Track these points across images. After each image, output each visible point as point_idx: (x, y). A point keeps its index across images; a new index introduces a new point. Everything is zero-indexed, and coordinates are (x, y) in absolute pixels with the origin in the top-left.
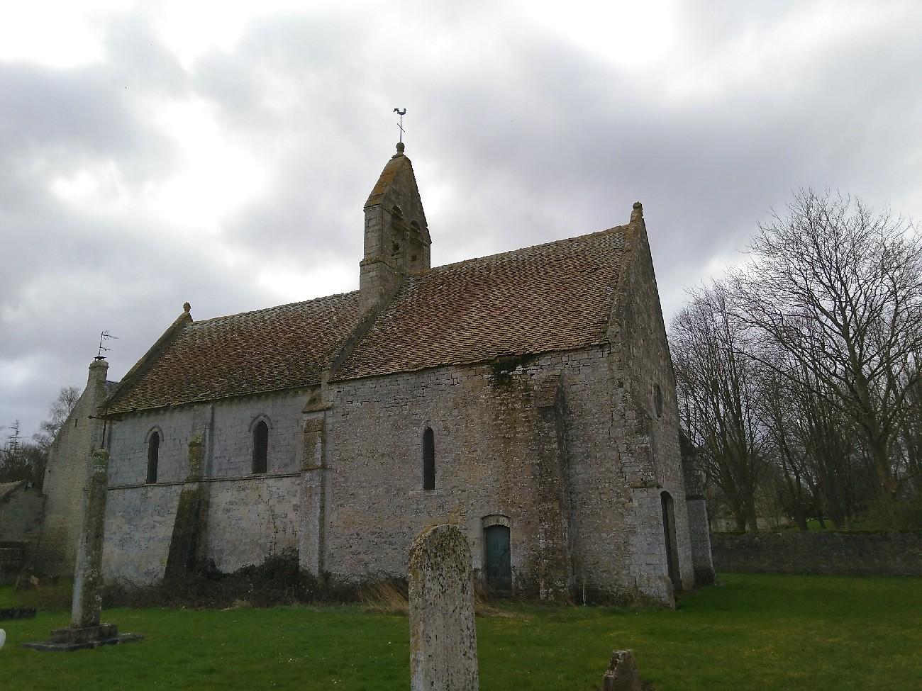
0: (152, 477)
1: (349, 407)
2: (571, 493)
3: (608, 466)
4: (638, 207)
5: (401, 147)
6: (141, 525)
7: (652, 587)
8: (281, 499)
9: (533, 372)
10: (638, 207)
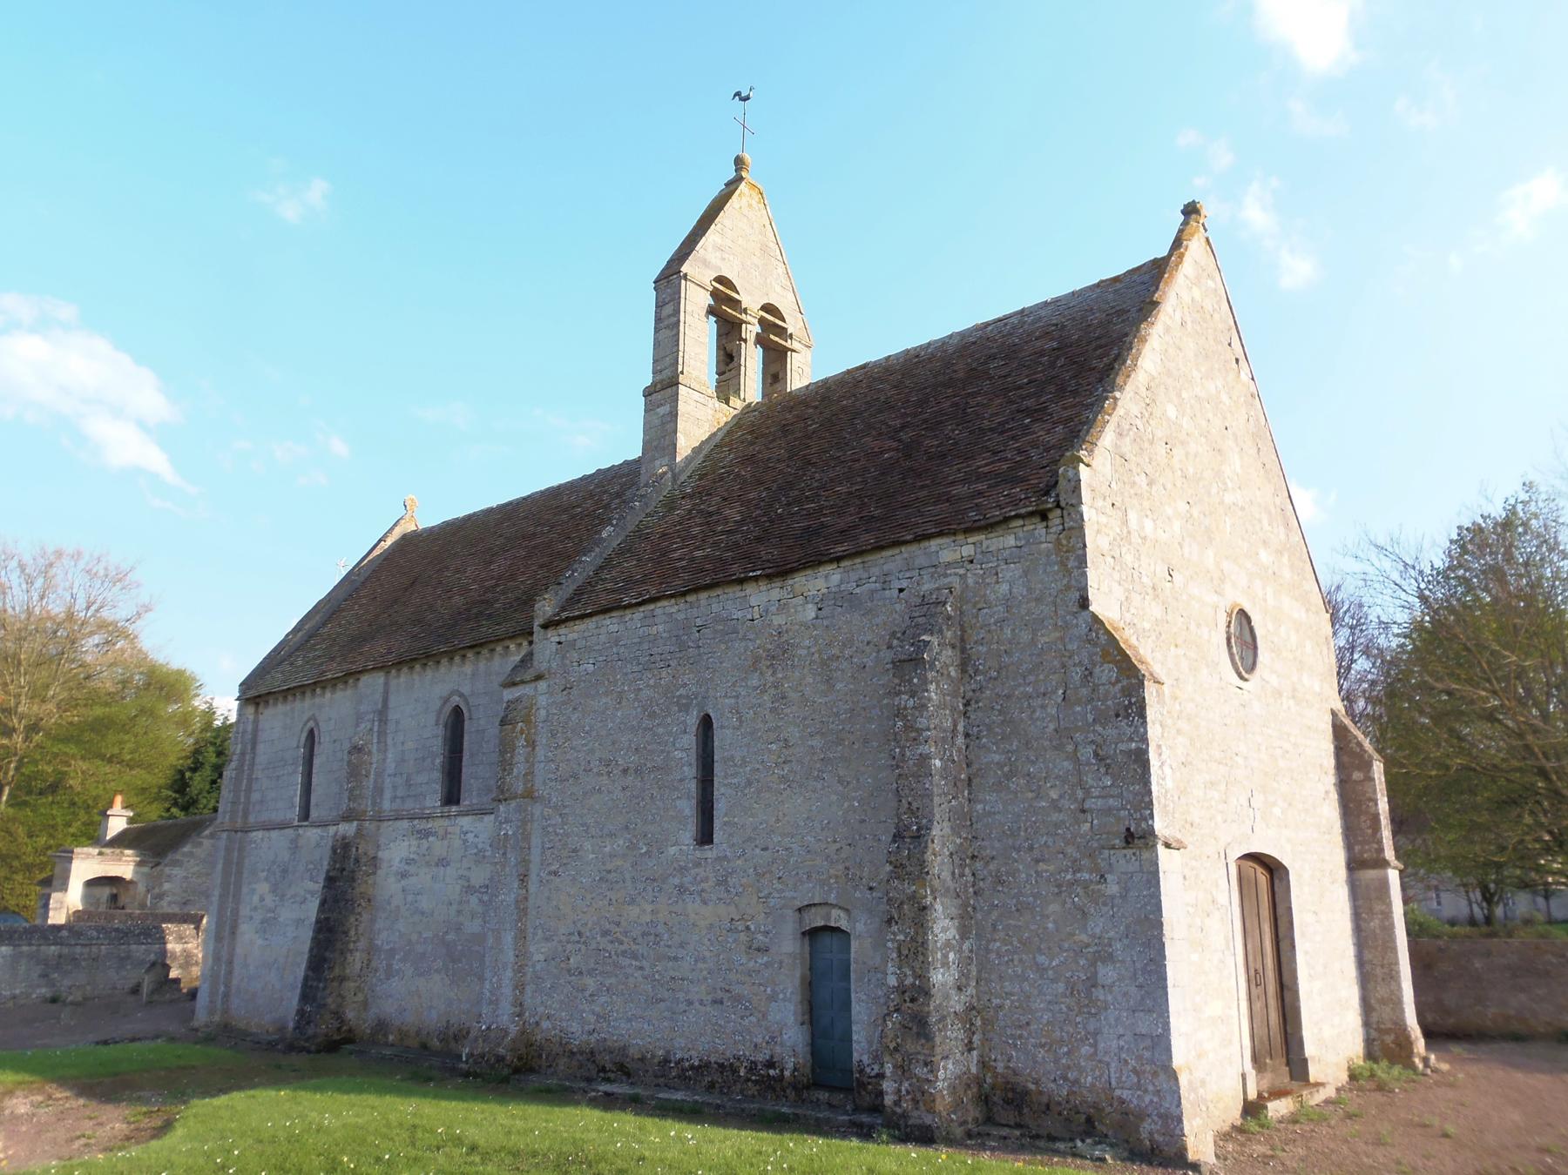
0: (305, 815)
3: (1054, 795)
7: (1146, 1091)
9: (904, 584)
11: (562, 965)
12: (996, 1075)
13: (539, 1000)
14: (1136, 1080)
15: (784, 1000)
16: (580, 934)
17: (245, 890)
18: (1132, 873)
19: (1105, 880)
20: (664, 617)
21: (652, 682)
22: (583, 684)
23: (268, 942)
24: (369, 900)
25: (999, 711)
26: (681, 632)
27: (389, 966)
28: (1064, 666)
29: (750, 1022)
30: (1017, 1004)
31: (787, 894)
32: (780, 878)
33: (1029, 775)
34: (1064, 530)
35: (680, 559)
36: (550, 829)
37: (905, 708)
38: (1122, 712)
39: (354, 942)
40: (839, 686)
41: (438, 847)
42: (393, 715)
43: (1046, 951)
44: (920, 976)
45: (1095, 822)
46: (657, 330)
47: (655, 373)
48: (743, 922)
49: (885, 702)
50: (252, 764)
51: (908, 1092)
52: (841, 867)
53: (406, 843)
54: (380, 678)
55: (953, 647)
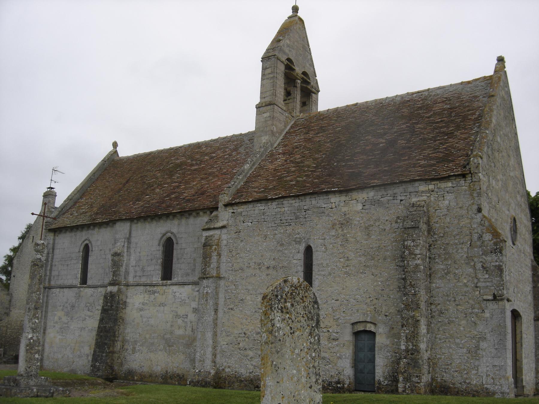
0: (84, 280)
1: (241, 226)
2: (431, 304)
4: (501, 60)
5: (295, 9)
7: (496, 385)
8: (183, 303)
9: (403, 198)
10: (501, 60)
11: (236, 346)
12: (437, 383)
13: (224, 360)
14: (493, 381)
15: (345, 358)
16: (245, 334)
17: (49, 314)
18: (495, 309)
19: (484, 312)
20: (288, 205)
21: (282, 231)
22: (246, 231)
23: (65, 337)
24: (123, 320)
25: (444, 249)
26: (296, 212)
27: (134, 348)
28: (471, 233)
29: (329, 367)
30: (447, 357)
31: (347, 318)
32: (344, 312)
33: (455, 273)
34: (472, 182)
35: (291, 181)
36: (229, 291)
37: (410, 246)
38: (493, 251)
39: (118, 337)
40: (373, 237)
42: (133, 240)
43: (460, 338)
44: (415, 346)
45: (481, 291)
46: (262, 79)
47: (261, 98)
48: (326, 329)
49: (394, 244)
50: (52, 258)
51: (409, 387)
52: (373, 307)
53: (142, 296)
54: (127, 225)
55: (426, 224)
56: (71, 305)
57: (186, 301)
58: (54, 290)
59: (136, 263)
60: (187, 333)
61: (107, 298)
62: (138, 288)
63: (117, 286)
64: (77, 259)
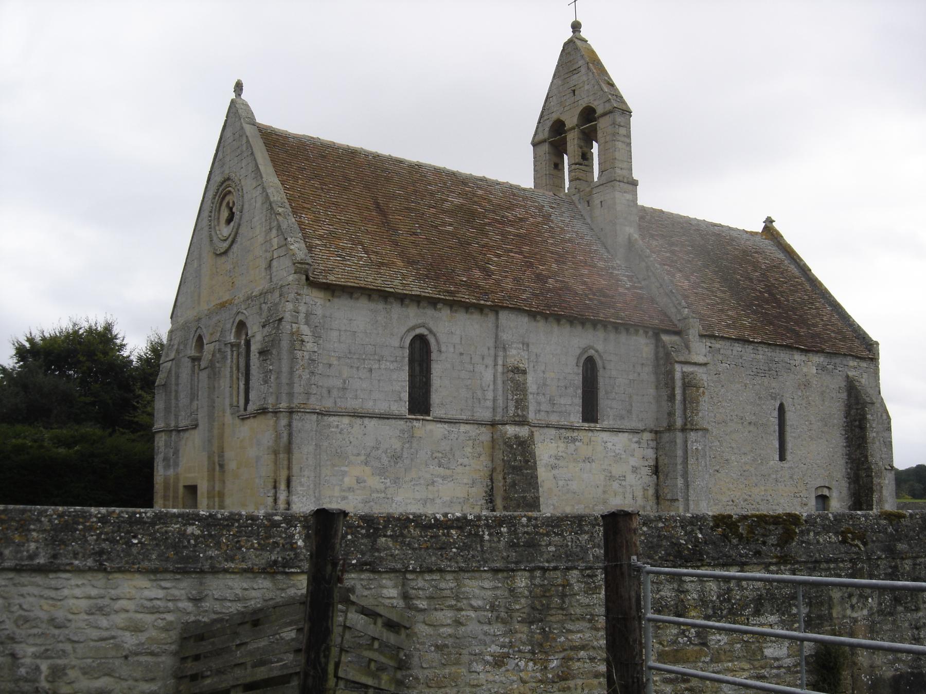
5: (576, 27)
6: (407, 479)
8: (617, 458)
16: (733, 501)
36: (714, 448)
41: (585, 450)
53: (554, 445)
56: (389, 455)
57: (622, 456)
58: (332, 419)
59: (538, 388)
60: (626, 502)
61: (511, 447)
62: (546, 430)
63: (527, 427)
64: (396, 361)
